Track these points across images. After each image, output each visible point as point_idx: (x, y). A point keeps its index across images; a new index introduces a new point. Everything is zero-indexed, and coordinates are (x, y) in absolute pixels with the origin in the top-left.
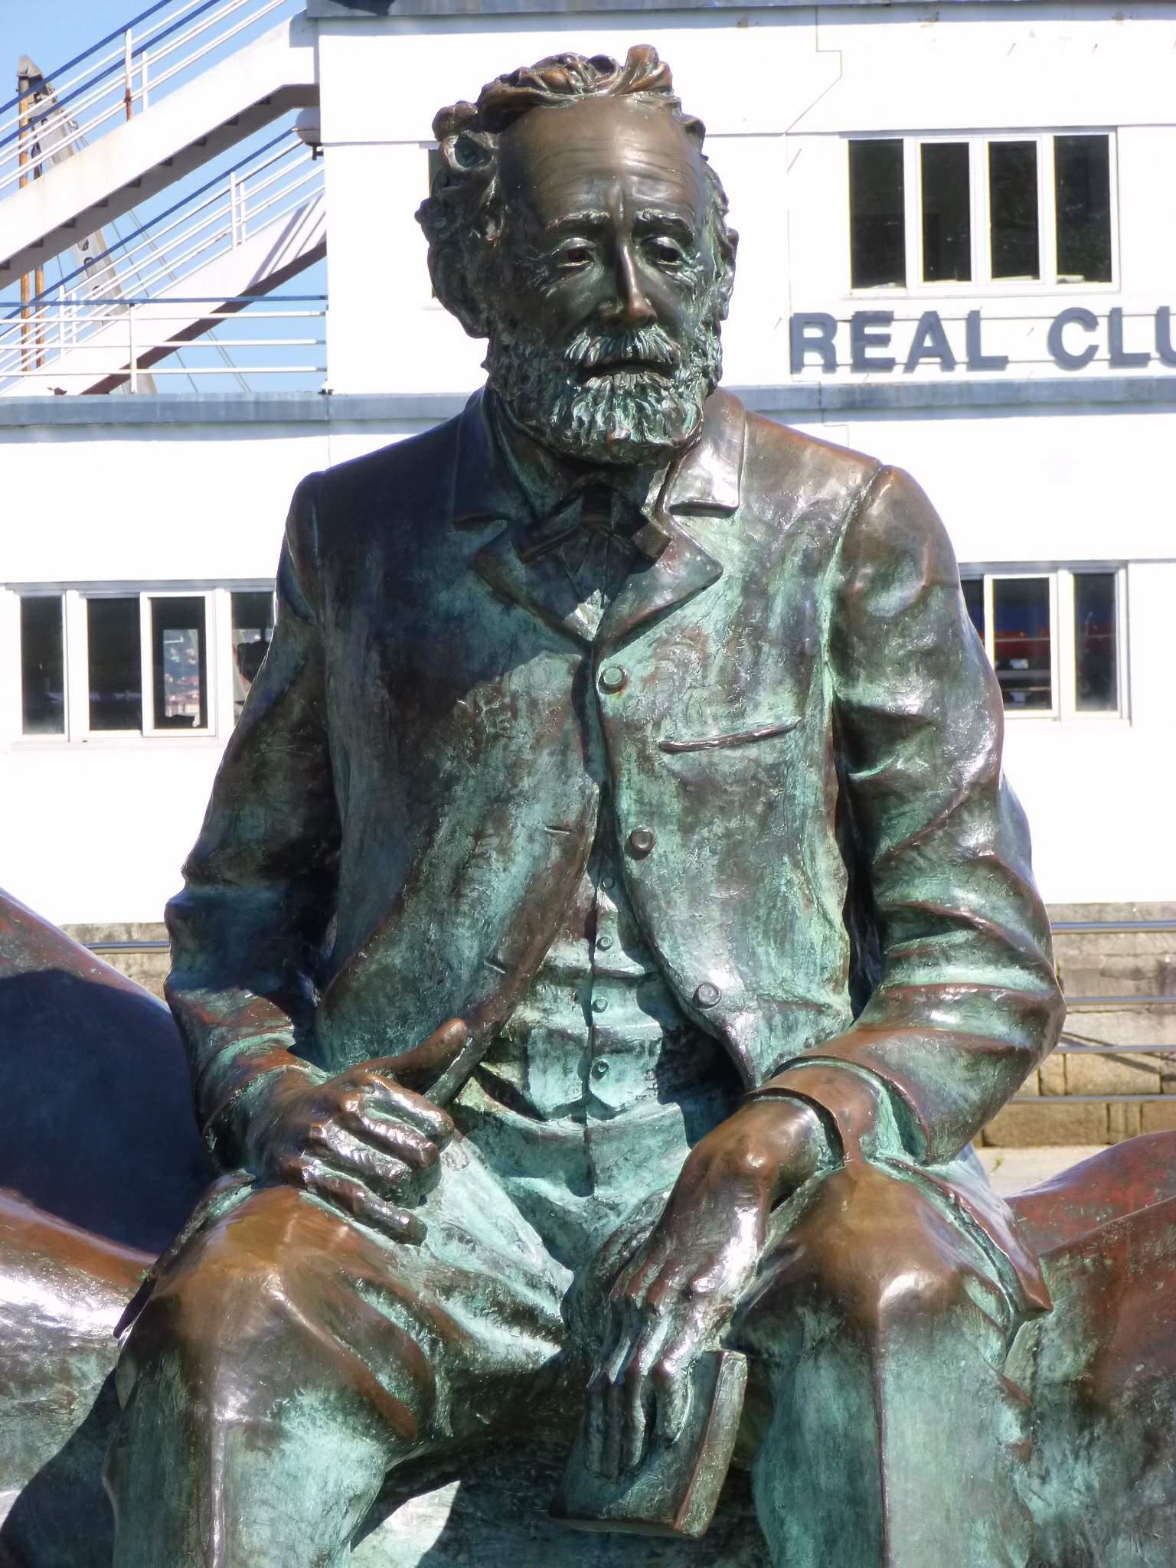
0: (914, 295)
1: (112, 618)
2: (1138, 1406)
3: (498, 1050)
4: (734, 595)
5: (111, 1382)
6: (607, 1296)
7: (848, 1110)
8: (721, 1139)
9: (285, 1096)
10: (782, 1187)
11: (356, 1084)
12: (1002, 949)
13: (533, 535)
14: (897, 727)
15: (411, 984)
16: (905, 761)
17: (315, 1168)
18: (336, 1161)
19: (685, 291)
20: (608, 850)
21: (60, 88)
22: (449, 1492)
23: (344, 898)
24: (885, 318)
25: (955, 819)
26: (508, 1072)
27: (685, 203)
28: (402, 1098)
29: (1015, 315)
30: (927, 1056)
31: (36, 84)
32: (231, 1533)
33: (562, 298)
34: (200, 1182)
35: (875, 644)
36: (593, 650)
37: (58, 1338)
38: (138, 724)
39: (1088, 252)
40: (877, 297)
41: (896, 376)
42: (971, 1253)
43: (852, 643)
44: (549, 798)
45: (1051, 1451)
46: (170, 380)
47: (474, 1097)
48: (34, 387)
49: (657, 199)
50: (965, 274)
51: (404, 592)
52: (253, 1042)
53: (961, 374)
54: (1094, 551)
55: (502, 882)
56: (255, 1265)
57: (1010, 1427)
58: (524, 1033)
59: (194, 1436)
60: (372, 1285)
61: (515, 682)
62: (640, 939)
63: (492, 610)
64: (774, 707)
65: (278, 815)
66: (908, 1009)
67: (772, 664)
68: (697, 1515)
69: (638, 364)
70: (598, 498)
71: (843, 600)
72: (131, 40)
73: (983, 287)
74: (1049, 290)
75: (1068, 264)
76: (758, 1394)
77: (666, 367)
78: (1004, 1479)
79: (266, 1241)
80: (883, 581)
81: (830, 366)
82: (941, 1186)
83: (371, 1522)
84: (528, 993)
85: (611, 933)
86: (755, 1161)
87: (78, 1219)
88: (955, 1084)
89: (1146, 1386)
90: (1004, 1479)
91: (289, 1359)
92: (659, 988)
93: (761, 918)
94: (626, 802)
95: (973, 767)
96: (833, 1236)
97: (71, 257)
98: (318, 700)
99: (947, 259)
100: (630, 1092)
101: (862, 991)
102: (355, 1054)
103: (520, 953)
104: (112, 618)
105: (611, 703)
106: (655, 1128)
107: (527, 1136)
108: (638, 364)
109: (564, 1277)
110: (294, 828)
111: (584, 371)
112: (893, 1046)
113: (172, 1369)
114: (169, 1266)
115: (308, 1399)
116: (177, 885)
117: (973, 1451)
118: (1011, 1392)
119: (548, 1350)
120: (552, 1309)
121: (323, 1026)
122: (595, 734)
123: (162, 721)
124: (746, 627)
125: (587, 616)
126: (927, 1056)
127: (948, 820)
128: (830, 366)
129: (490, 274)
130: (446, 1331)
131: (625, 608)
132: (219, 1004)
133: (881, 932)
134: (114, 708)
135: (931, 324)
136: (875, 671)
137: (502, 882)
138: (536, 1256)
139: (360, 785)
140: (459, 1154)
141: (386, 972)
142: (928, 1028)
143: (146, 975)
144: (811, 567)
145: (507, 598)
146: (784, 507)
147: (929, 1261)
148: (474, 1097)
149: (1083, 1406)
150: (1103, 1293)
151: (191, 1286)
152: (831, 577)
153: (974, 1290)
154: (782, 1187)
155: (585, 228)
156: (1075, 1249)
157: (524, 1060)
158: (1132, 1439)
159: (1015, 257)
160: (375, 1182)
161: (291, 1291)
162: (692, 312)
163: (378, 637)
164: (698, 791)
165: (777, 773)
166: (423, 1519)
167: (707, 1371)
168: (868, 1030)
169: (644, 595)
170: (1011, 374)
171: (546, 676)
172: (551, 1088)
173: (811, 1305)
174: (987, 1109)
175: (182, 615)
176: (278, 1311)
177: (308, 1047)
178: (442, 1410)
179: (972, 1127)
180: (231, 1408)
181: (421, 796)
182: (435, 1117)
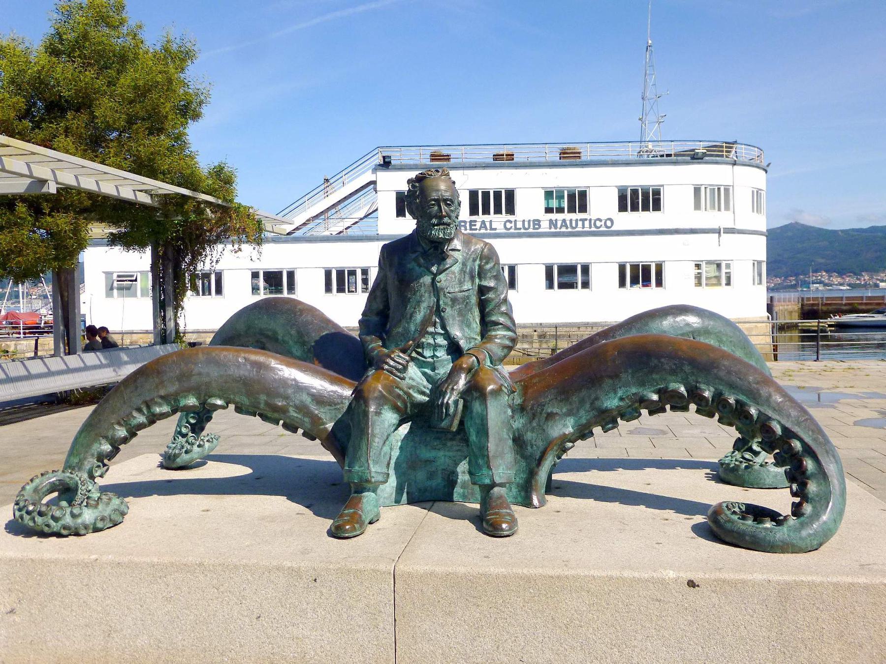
0: (480, 217)
1: (340, 273)
2: (531, 409)
3: (418, 347)
4: (461, 265)
5: (350, 404)
6: (438, 389)
7: (481, 357)
8: (459, 362)
9: (380, 354)
10: (469, 370)
11: (393, 352)
12: (508, 329)
13: (425, 254)
14: (489, 289)
15: (403, 335)
16: (491, 295)
17: (386, 367)
18: (390, 366)
19: (452, 211)
20: (438, 310)
21: (331, 181)
22: (410, 424)
23: (390, 319)
24: (475, 221)
25: (499, 306)
26: (420, 350)
27: (452, 196)
28: (401, 354)
29: (498, 221)
30: (495, 348)
31: (327, 180)
32: (372, 431)
33: (430, 213)
34: (365, 369)
35: (485, 274)
36: (435, 275)
37: (341, 397)
38: (135, 295)
39: (511, 210)
40: (474, 218)
41: (477, 232)
42: (503, 382)
43: (481, 274)
44: (427, 301)
45: (516, 417)
46: (354, 231)
47: (414, 355)
48: (327, 233)
49: (447, 195)
50: (489, 214)
51: (401, 265)
52: (375, 345)
53: (489, 231)
54: (659, 259)
55: (419, 317)
56: (376, 384)
57: (509, 412)
58: (423, 343)
59: (366, 414)
60: (397, 387)
61: (421, 281)
62: (444, 327)
63: (417, 268)
64: (467, 285)
65: (379, 305)
66: (491, 339)
67: (467, 278)
68: (454, 428)
69: (444, 224)
70: (436, 248)
71: (480, 266)
72: (344, 173)
73: (492, 216)
74: (504, 217)
75: (507, 212)
76: (465, 406)
77: (449, 225)
78: (509, 422)
79: (377, 379)
80: (487, 263)
81: (466, 229)
82: (497, 370)
83: (396, 429)
84: (423, 336)
85: (438, 326)
86: (464, 366)
87: (343, 376)
88: (500, 352)
89: (533, 405)
90: (509, 422)
91: (382, 400)
92: (447, 336)
93: (465, 323)
94: (441, 302)
95: (502, 296)
96: (479, 379)
97: (333, 211)
98: (386, 284)
99: (486, 211)
100: (441, 354)
101: (483, 336)
102: (393, 347)
103: (422, 329)
104: (340, 273)
105: (438, 284)
106: (446, 360)
107: (424, 362)
108: (444, 224)
109: (430, 386)
110: (381, 307)
111: (434, 225)
112: (488, 346)
113: (362, 402)
114: (360, 384)
115: (386, 407)
116: (361, 317)
117: (503, 416)
118: (510, 406)
119: (427, 399)
120: (428, 392)
121: (387, 342)
122: (435, 290)
123: (349, 291)
124: (462, 271)
125: (434, 269)
126: (495, 348)
127: (498, 305)
128: (466, 229)
129: (417, 208)
130: (409, 395)
131: (441, 268)
132: (368, 338)
133: (486, 325)
134: (341, 289)
135: (483, 222)
136: (485, 279)
137: (419, 317)
138: (425, 383)
139: (393, 300)
140: (411, 364)
141: (398, 333)
142: (495, 342)
143: (356, 335)
144: (474, 260)
145: (420, 266)
146: (469, 250)
147: (496, 383)
148: (414, 355)
149: (522, 409)
150: (525, 389)
151: (365, 387)
152: (478, 262)
153: (503, 388)
154: (469, 370)
155: (434, 200)
156: (520, 381)
157: (423, 348)
158: (530, 415)
159: (498, 211)
160: (397, 369)
161: (383, 388)
162: (453, 215)
163: (397, 273)
164: (454, 300)
165: (468, 297)
166: (405, 429)
167: (456, 403)
168: (484, 343)
169: (444, 265)
170: (497, 231)
171: (427, 279)
172: (428, 353)
173: (475, 391)
174: (505, 356)
175: (352, 273)
176: (380, 392)
177: (384, 346)
178: (409, 409)
179: (501, 360)
180: (372, 409)
181: (404, 301)
182: (407, 358)
